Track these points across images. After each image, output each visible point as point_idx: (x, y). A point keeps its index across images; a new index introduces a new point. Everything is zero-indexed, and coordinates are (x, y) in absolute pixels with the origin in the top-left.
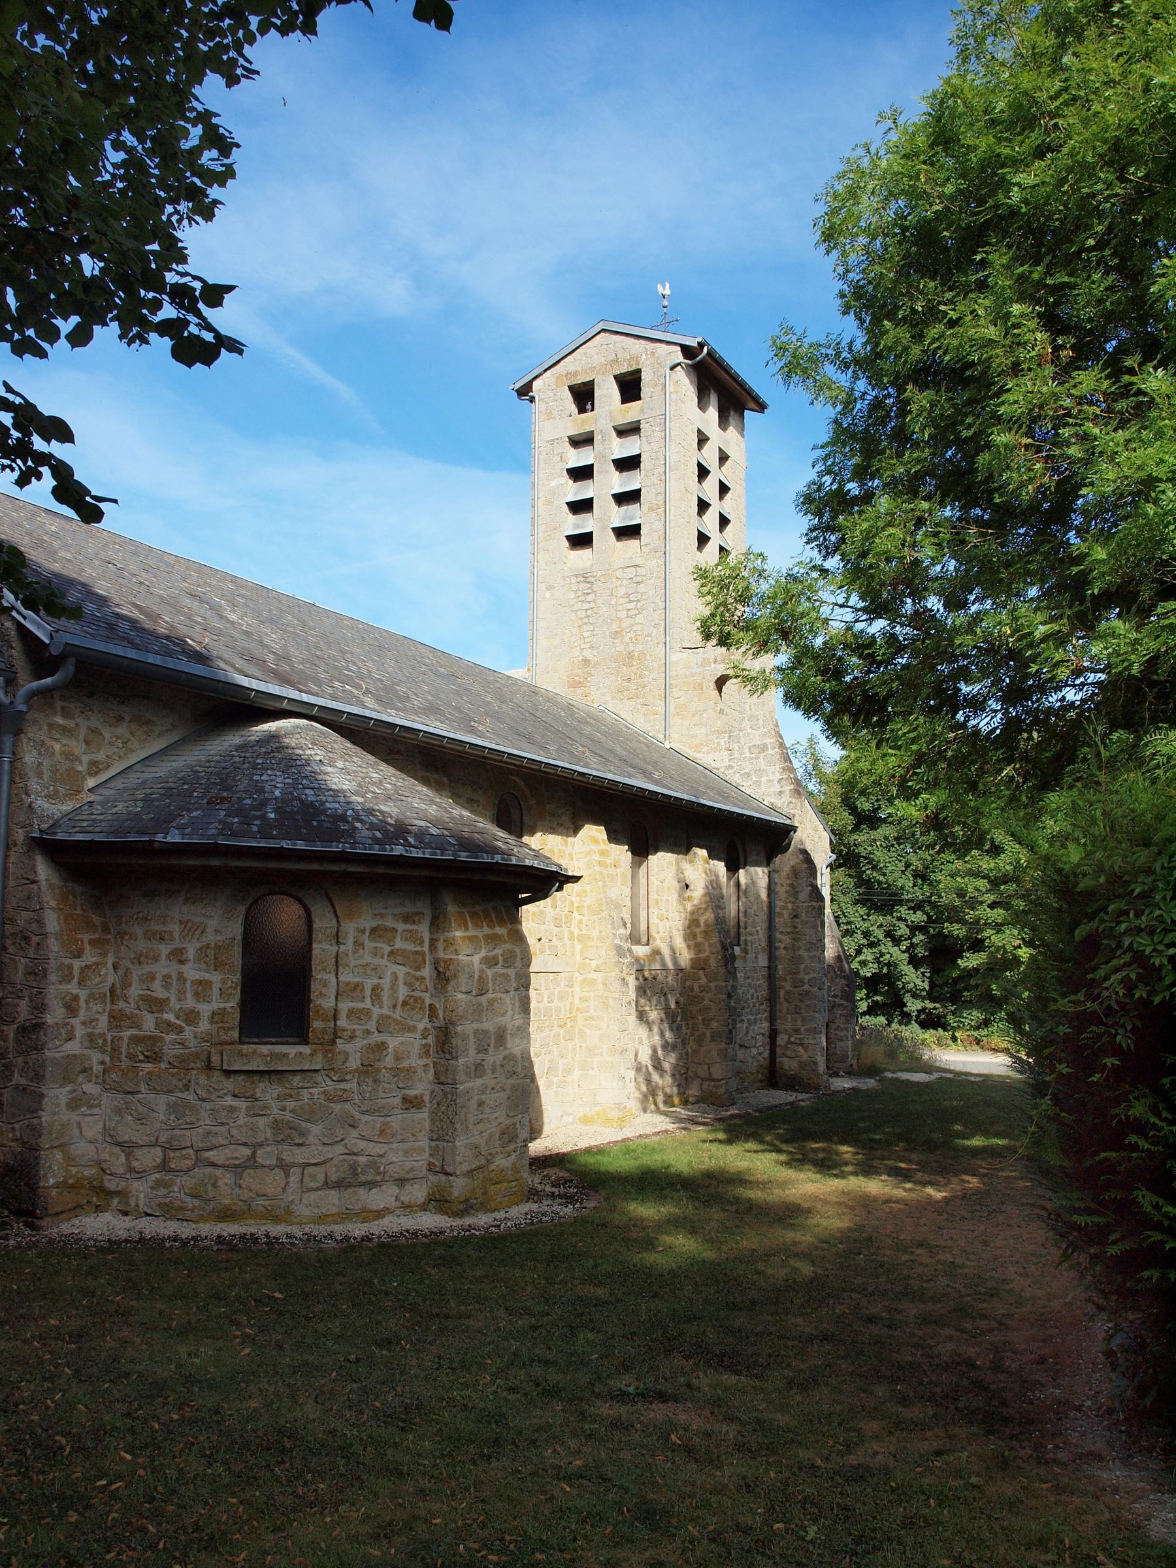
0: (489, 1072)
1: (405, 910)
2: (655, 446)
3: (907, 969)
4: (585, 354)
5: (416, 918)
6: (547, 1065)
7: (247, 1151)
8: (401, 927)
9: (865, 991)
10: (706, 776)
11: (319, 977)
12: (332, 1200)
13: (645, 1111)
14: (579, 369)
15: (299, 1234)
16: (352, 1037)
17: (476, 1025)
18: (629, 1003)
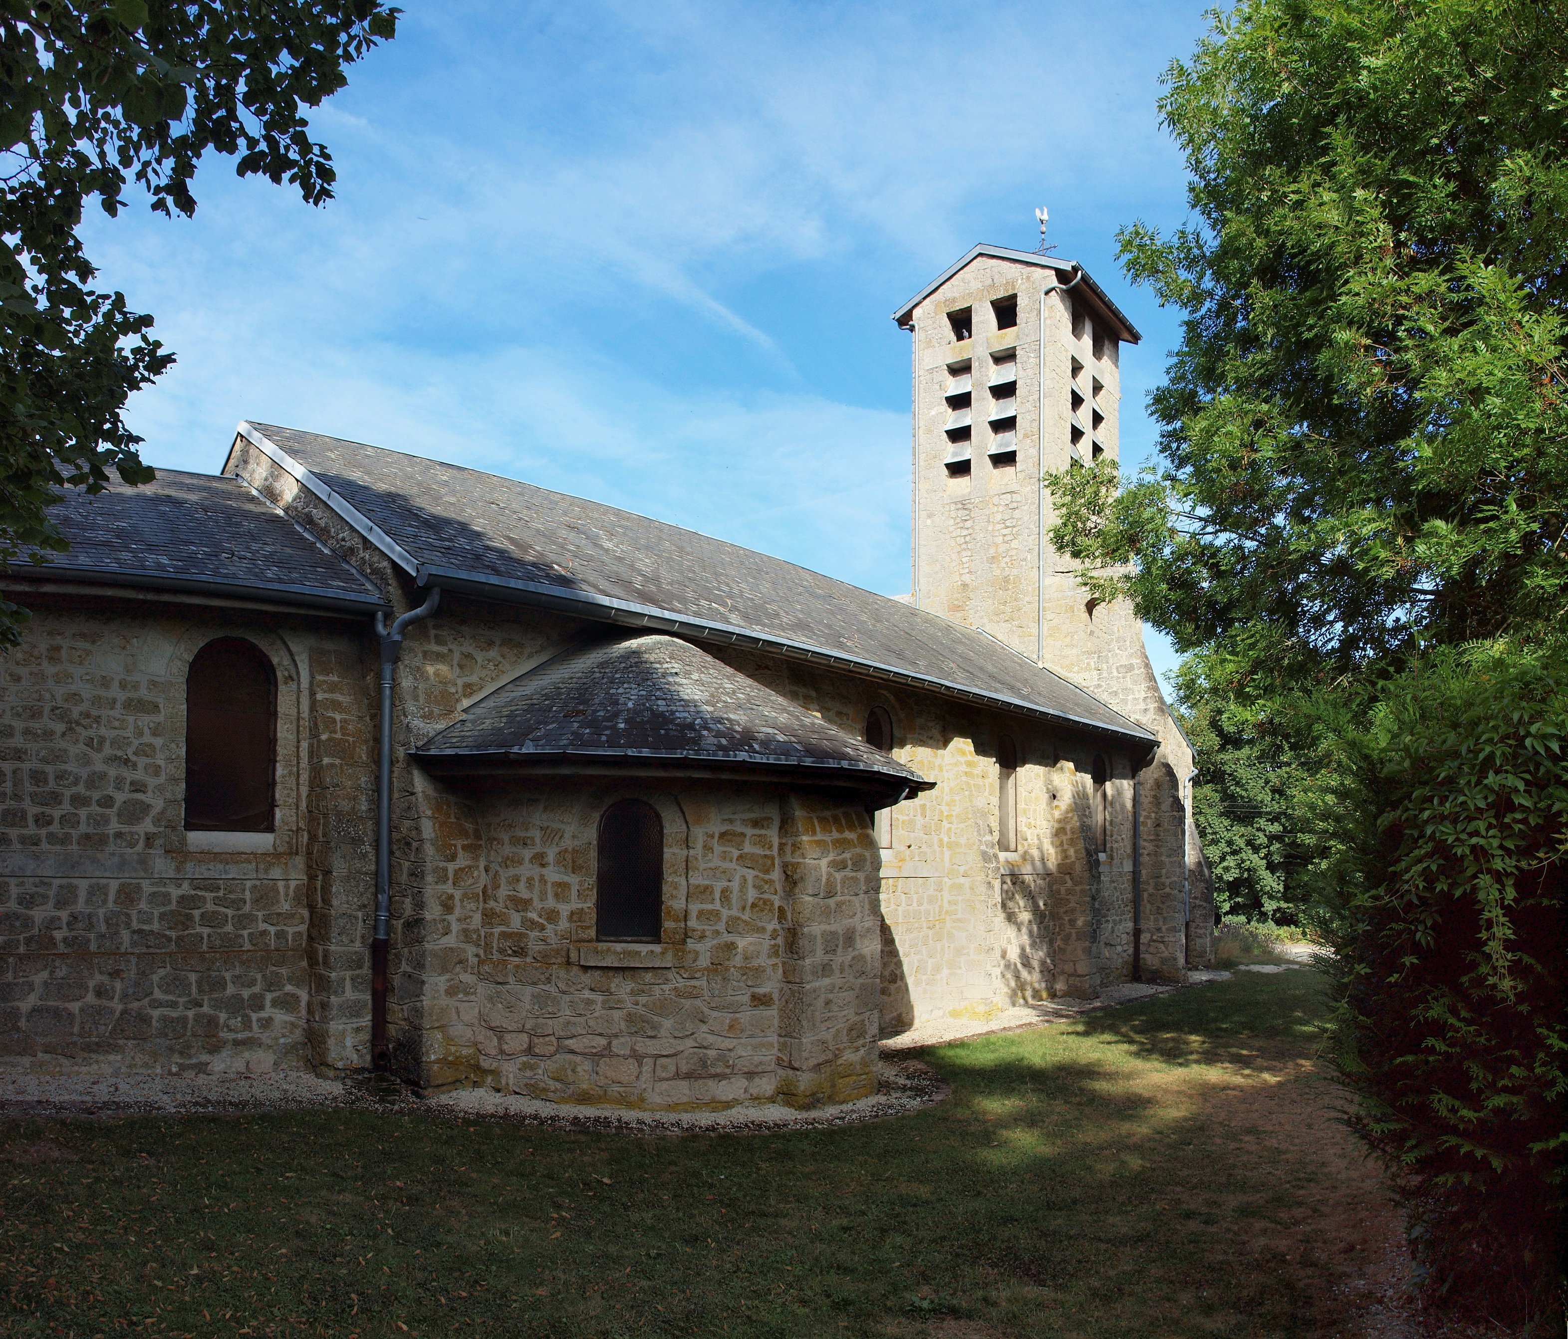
0: (837, 972)
1: (752, 815)
2: (1030, 372)
3: (1265, 874)
4: (963, 280)
5: (765, 823)
6: (916, 964)
7: (603, 1041)
8: (749, 831)
9: (1227, 894)
10: (1076, 694)
11: (670, 879)
12: (683, 1090)
13: (1014, 1005)
14: (957, 295)
15: (648, 1121)
16: (702, 937)
17: (824, 927)
18: (995, 905)
